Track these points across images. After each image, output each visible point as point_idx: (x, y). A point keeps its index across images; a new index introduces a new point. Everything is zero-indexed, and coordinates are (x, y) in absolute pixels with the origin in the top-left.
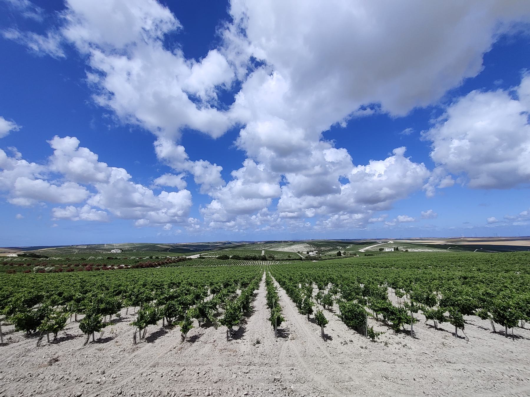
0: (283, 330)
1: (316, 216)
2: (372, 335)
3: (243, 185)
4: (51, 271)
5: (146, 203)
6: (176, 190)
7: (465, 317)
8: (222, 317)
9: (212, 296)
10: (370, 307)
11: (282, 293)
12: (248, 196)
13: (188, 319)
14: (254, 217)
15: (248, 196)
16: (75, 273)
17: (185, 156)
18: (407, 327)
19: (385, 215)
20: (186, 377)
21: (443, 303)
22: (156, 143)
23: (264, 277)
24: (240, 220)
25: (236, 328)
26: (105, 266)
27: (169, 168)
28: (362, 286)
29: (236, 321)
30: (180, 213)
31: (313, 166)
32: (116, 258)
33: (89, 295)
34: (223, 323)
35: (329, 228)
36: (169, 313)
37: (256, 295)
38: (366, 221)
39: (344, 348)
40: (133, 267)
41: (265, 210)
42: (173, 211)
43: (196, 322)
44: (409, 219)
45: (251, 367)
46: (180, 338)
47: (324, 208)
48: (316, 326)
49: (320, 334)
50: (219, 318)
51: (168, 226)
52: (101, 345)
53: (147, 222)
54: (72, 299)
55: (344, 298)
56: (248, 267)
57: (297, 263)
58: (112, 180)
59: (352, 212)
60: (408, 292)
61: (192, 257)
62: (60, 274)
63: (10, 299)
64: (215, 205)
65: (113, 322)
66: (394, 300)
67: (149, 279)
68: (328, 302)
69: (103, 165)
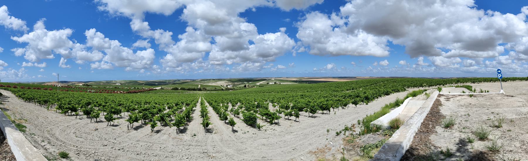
0: (210, 129)
1: (233, 64)
2: (259, 128)
3: (186, 43)
5: (130, 58)
6: (145, 49)
7: (300, 113)
8: (174, 122)
9: (168, 110)
10: (259, 114)
11: (210, 109)
12: (190, 51)
13: (154, 122)
14: (194, 64)
15: (190, 51)
17: (148, 27)
18: (276, 121)
19: (271, 64)
20: (154, 148)
21: (293, 108)
22: (131, 23)
23: (200, 100)
24: (185, 66)
25: (182, 128)
27: (139, 36)
28: (256, 103)
29: (182, 124)
30: (148, 62)
31: (233, 32)
33: (108, 104)
34: (174, 125)
35: (241, 70)
36: (145, 117)
37: (195, 110)
38: (261, 67)
39: (244, 136)
40: (127, 93)
41: (200, 59)
42: (144, 61)
43: (159, 124)
44: (283, 67)
45: (190, 147)
46: (151, 131)
47: (238, 59)
48: (229, 126)
49: (231, 130)
50: (172, 122)
51: (142, 71)
52: (114, 128)
53: (131, 69)
55: (246, 110)
56: (190, 94)
57: (220, 92)
58: (112, 47)
59: (254, 61)
60: (278, 104)
61: (157, 88)
64: (169, 57)
65: (118, 118)
66: (271, 109)
67: (135, 99)
68: (237, 113)
69: (107, 39)
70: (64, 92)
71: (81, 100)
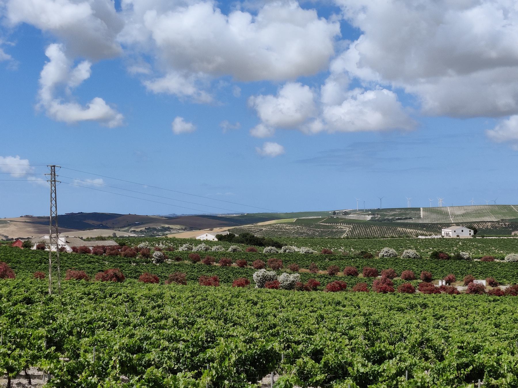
4: (291, 286)
16: (349, 295)
26: (428, 279)
32: (459, 258)
33: (390, 366)
54: (346, 374)
62: (314, 294)
63: (209, 353)
70: (95, 285)
71: (212, 338)
